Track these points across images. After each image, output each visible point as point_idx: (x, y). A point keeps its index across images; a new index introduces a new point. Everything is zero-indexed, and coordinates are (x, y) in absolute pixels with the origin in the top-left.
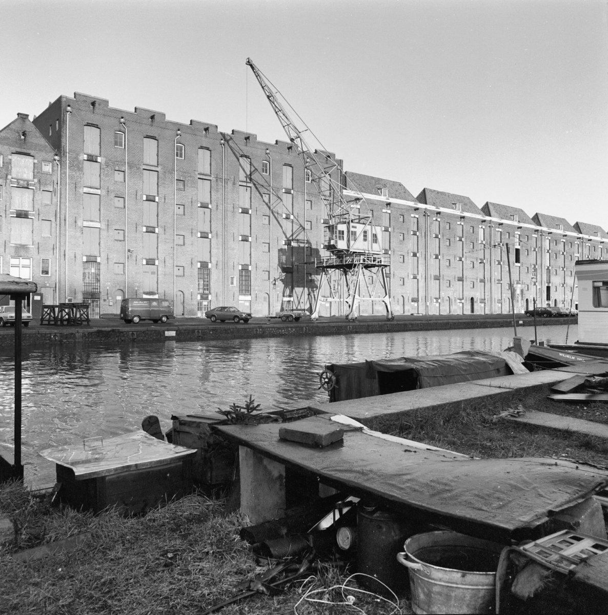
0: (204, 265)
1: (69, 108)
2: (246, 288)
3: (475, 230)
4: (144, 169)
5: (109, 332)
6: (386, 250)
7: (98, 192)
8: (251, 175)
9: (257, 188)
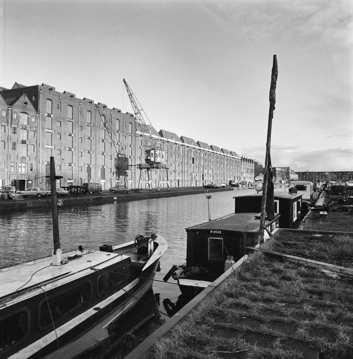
0: (89, 166)
1: (41, 91)
2: (103, 177)
3: (172, 147)
4: (87, 125)
5: (99, 198)
6: (167, 160)
7: (51, 131)
8: (105, 124)
9: (107, 130)
